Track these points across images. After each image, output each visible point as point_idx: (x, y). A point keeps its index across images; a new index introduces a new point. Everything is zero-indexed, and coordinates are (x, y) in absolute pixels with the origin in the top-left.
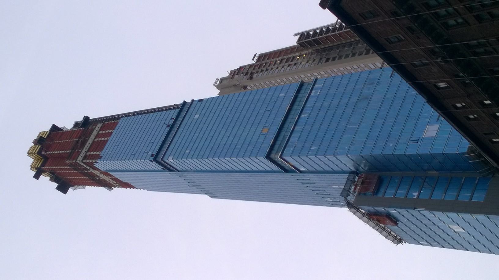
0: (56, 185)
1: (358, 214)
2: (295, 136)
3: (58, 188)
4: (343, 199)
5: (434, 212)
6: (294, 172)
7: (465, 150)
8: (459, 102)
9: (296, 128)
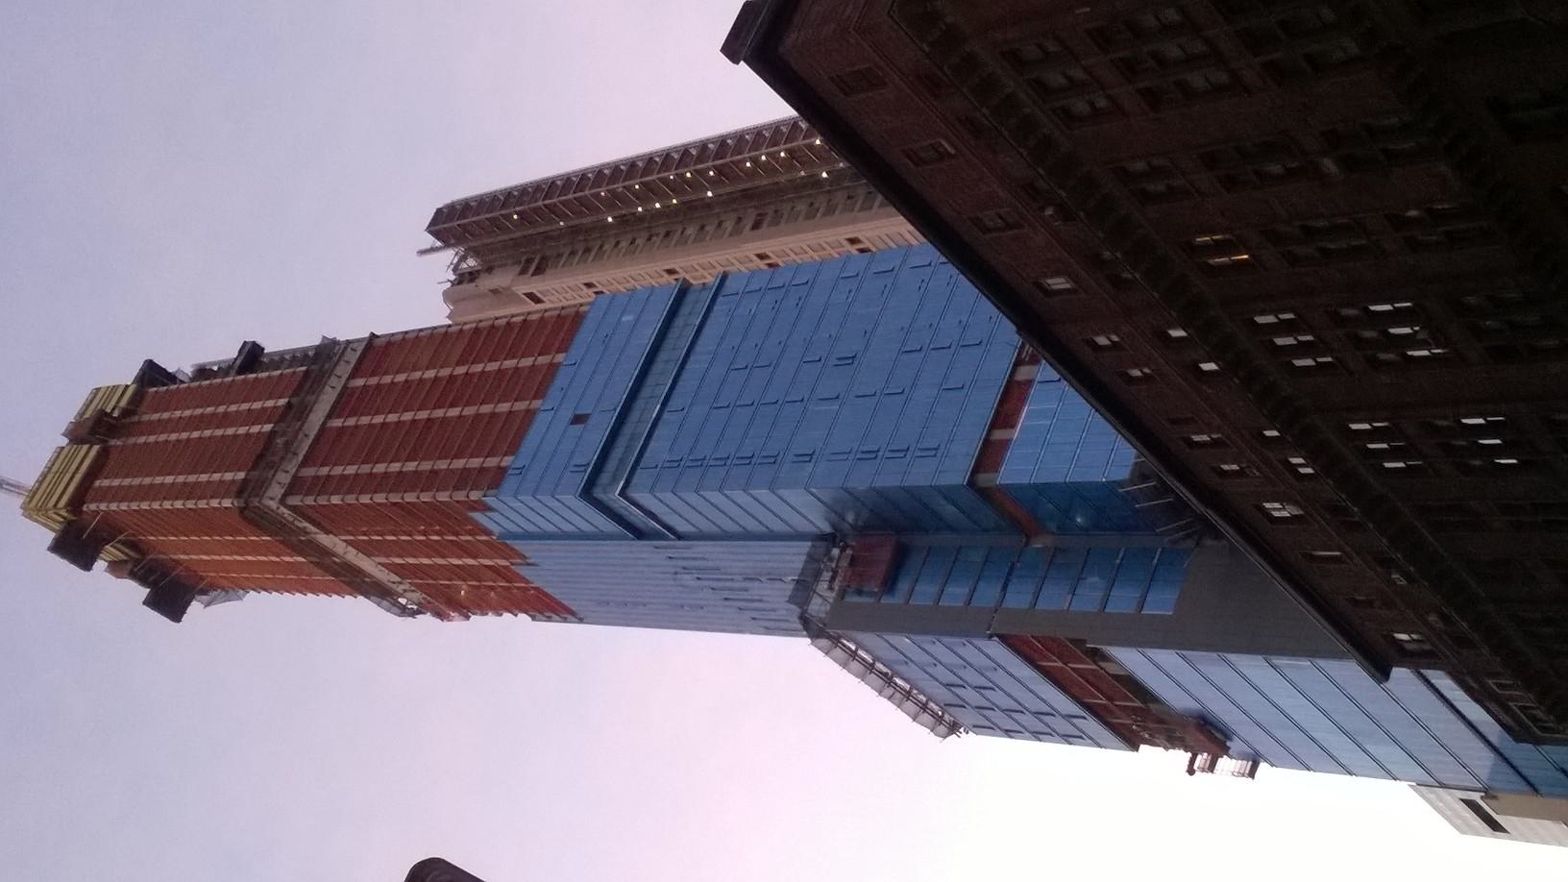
1: (838, 652)
3: (152, 602)
4: (797, 610)
5: (1281, 661)
6: (663, 537)
7: (1123, 473)
8: (1102, 332)
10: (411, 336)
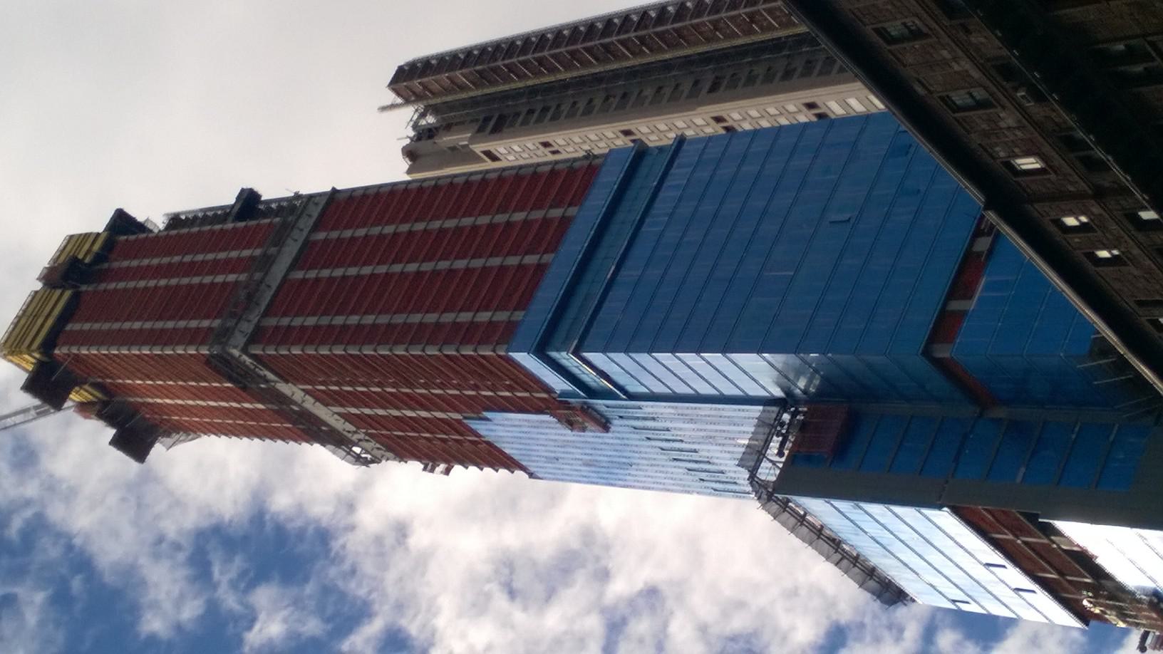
0: (111, 432)
2: (619, 295)
3: (117, 442)
8: (1075, 214)
9: (623, 272)
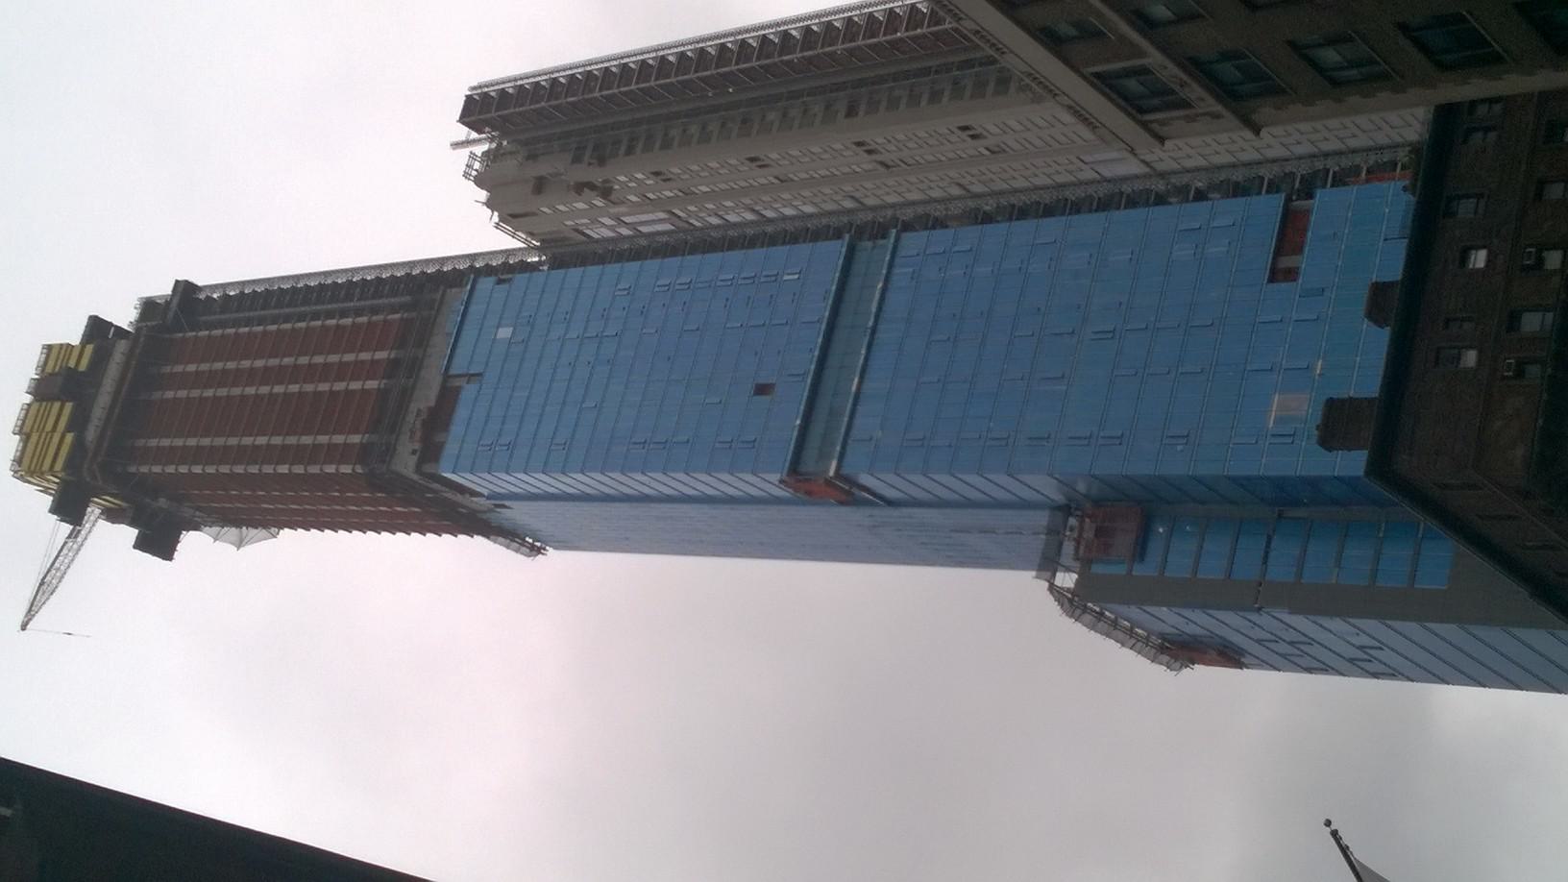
3: (141, 544)
6: (877, 505)
10: (1165, 658)
